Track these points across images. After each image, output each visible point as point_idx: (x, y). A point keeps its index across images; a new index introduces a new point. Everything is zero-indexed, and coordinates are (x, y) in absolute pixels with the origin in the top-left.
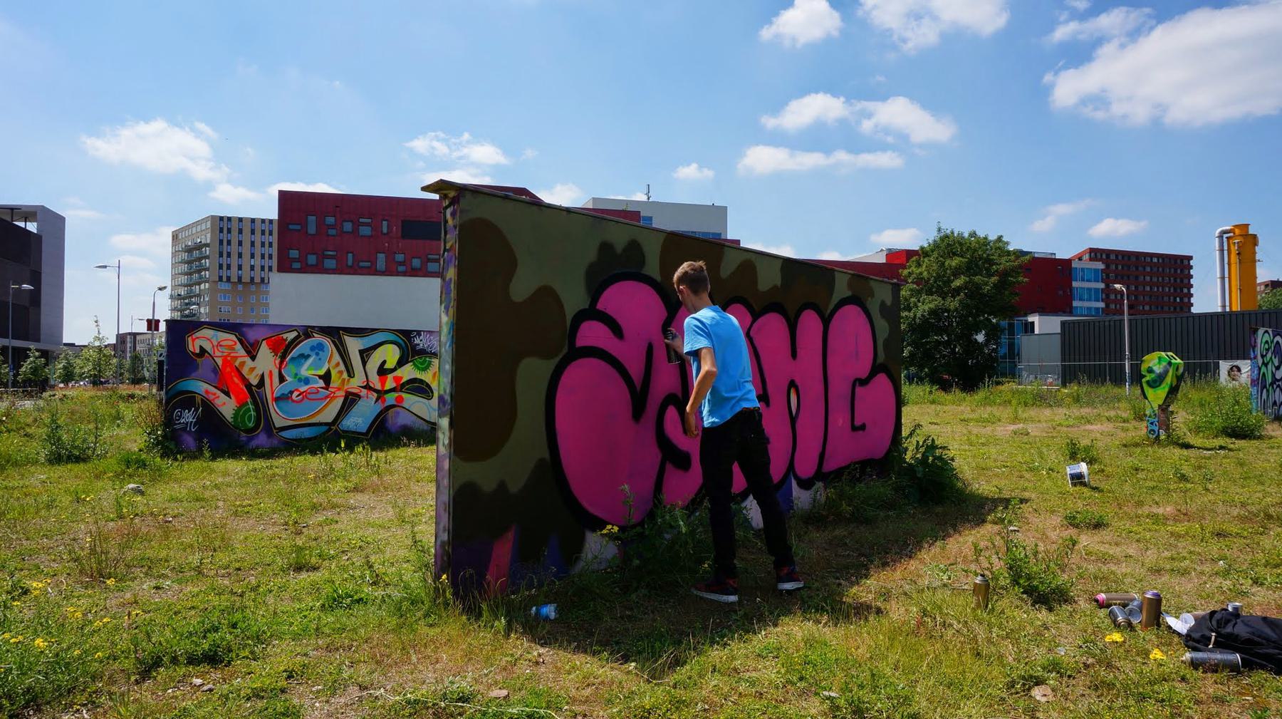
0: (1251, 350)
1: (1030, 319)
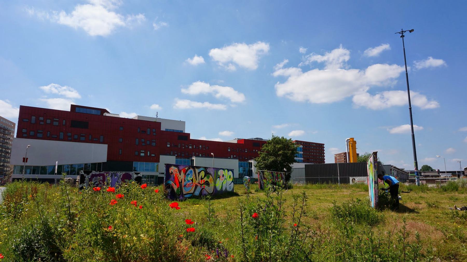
1: (250, 161)
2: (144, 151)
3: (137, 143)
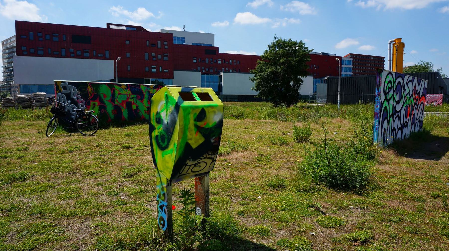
0: (376, 88)
2: (155, 67)
3: (147, 58)
